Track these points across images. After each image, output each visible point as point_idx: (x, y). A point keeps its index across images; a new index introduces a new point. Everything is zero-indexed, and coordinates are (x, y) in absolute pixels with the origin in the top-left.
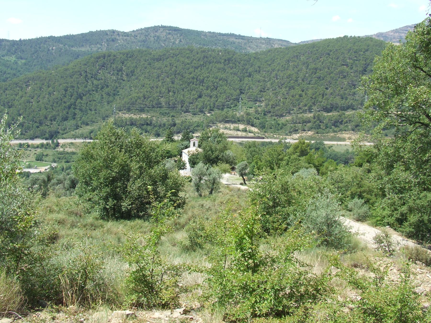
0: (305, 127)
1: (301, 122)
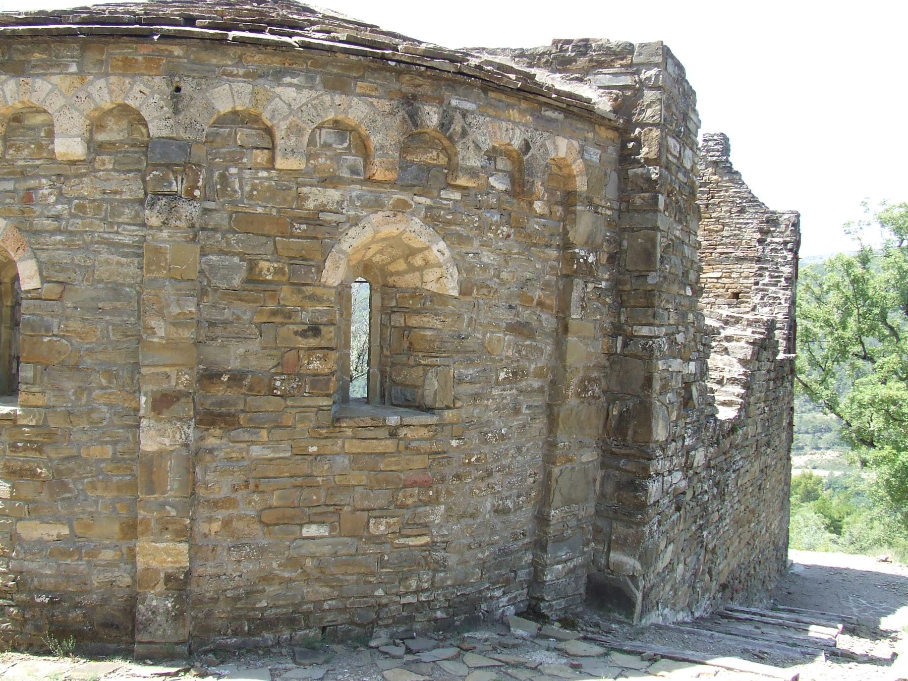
0: (819, 441)
1: (810, 431)
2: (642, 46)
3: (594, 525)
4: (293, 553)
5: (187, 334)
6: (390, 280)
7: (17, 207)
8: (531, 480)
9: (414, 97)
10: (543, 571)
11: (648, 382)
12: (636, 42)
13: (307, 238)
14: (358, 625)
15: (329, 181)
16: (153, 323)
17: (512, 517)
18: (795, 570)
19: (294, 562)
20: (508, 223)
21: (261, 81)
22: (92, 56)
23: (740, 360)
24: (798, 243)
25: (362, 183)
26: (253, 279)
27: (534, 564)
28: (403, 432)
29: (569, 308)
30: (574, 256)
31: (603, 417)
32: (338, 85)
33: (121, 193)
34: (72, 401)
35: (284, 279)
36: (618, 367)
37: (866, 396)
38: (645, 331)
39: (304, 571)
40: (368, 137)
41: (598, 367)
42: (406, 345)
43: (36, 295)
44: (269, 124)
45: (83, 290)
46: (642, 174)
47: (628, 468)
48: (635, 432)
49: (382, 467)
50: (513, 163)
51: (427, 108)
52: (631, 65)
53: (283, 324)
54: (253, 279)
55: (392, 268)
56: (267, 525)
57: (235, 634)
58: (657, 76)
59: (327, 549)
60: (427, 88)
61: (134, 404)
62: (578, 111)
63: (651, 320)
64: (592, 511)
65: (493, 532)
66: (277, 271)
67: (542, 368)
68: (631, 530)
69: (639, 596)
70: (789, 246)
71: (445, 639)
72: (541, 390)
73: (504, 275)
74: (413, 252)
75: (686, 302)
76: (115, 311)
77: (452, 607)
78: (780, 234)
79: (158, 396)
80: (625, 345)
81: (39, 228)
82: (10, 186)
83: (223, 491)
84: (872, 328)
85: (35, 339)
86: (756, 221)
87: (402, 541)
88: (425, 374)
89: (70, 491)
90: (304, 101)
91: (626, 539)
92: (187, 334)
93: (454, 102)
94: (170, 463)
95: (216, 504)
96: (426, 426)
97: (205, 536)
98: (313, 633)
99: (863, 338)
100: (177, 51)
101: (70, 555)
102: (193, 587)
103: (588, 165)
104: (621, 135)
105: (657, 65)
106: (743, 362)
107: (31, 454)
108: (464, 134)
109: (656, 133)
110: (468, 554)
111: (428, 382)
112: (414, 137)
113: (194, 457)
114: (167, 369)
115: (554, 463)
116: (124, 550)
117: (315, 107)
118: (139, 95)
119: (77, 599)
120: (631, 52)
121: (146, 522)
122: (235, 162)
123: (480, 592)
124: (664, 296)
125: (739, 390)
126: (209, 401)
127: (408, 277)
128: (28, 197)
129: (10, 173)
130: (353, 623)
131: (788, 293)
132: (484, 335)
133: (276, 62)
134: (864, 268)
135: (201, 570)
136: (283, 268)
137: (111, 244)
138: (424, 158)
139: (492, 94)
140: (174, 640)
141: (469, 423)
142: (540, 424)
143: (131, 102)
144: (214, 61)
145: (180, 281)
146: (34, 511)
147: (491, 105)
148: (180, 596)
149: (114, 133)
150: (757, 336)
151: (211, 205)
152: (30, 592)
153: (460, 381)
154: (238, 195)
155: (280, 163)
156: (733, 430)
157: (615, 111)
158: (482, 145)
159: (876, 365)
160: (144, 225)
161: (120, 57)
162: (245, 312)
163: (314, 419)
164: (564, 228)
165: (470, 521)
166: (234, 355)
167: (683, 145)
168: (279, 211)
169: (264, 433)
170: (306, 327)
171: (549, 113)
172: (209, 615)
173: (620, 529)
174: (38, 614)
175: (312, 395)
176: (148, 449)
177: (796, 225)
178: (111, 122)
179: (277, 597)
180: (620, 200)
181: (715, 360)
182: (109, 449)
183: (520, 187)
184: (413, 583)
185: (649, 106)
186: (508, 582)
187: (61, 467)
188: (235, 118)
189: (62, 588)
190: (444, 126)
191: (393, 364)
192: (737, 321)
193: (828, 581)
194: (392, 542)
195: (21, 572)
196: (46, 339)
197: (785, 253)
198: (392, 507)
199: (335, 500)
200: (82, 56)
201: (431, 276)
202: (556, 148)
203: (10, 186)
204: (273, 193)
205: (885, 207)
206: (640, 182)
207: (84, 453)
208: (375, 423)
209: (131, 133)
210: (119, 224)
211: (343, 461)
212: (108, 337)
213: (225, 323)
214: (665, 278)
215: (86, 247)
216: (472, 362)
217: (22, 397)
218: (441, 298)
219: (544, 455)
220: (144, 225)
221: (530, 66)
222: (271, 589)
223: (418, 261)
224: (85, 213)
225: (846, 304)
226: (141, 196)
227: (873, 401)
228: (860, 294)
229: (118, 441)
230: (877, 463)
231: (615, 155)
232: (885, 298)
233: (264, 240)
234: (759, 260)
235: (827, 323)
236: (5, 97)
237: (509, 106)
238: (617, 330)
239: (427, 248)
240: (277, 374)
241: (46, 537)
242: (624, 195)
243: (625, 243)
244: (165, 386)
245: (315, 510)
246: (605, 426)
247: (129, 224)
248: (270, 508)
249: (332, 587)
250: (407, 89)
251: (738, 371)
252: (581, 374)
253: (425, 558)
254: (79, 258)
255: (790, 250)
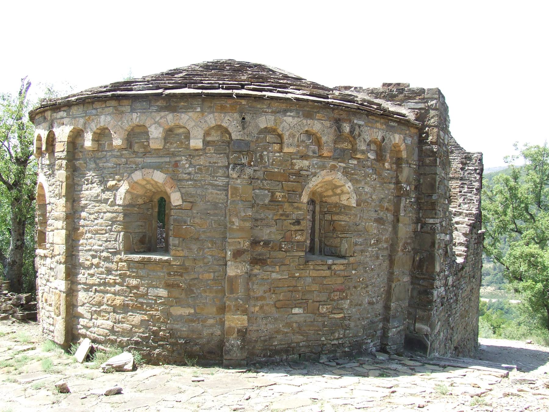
2: (429, 90)
3: (408, 311)
4: (288, 321)
5: (248, 224)
6: (324, 199)
7: (171, 169)
8: (383, 289)
9: (339, 120)
10: (388, 332)
11: (433, 244)
12: (426, 87)
13: (295, 182)
14: (314, 353)
15: (304, 157)
16: (234, 220)
17: (375, 306)
18: (482, 348)
19: (289, 325)
20: (375, 173)
21: (278, 115)
22: (207, 104)
23: (463, 234)
24: (482, 170)
25: (317, 157)
26: (273, 200)
27: (383, 328)
28: (333, 267)
29: (399, 211)
30: (401, 188)
31: (412, 261)
32: (309, 116)
33: (218, 163)
34: (195, 254)
35: (286, 200)
36: (418, 238)
37: (517, 252)
38: (431, 221)
39: (293, 329)
40: (321, 138)
41: (411, 238)
42: (332, 228)
43: (179, 208)
44: (280, 133)
45: (201, 205)
46: (429, 149)
47: (424, 284)
48: (427, 268)
49: (325, 283)
50: (377, 146)
51: (345, 125)
52: (424, 99)
53: (285, 220)
54: (273, 200)
55: (325, 194)
56: (278, 308)
57: (264, 356)
58: (436, 104)
59: (302, 319)
60: (344, 116)
61: (223, 255)
62: (403, 122)
63: (434, 216)
64: (407, 304)
65: (368, 313)
66: (284, 197)
67: (387, 238)
68: (426, 313)
69: (429, 343)
70: (478, 171)
71: (351, 360)
72: (387, 248)
73: (374, 197)
74: (337, 187)
75: (445, 207)
76: (215, 215)
77: (351, 346)
78: (473, 162)
79: (235, 252)
80: (422, 227)
81: (181, 178)
82: (168, 160)
83: (260, 293)
84: (521, 215)
85: (179, 227)
86: (459, 158)
87: (332, 316)
88: (341, 242)
89: (194, 293)
90: (295, 123)
91: (423, 317)
92: (248, 224)
93: (355, 121)
94: (240, 281)
95: (257, 299)
96: (343, 264)
97: (253, 313)
98: (296, 356)
99: (516, 221)
100: (244, 102)
101: (194, 322)
102: (248, 336)
103: (407, 145)
104: (419, 130)
105: (436, 99)
106: (465, 235)
107: (177, 277)
108: (360, 135)
109: (436, 130)
110: (358, 322)
111: (342, 245)
112: (339, 136)
113: (250, 276)
114: (239, 240)
115: (393, 282)
116: (218, 319)
117: (300, 125)
118: (228, 121)
119: (197, 341)
120: (424, 92)
121: (229, 306)
122: (266, 149)
123: (363, 340)
124: (439, 205)
125: (463, 248)
126: (255, 254)
127: (333, 198)
128: (176, 165)
129: (167, 154)
130: (312, 352)
131: (478, 196)
132: (365, 224)
133: (284, 106)
134: (516, 182)
135: (250, 328)
136: (285, 196)
137: (213, 185)
138: (342, 146)
139: (370, 117)
140: (242, 358)
141: (359, 263)
142: (386, 264)
143: (224, 125)
144: (259, 106)
145: (245, 202)
146: (179, 302)
147: (369, 122)
148: (244, 339)
149: (214, 137)
150: (471, 222)
151: (256, 168)
152: (176, 338)
153: (356, 244)
154: (267, 164)
155: (286, 150)
156: (463, 268)
157: (416, 120)
158: (366, 140)
159: (522, 236)
160: (228, 177)
161: (219, 105)
162: (270, 214)
163: (297, 261)
164: (397, 174)
165: (360, 307)
166: (265, 234)
167: (445, 133)
168: (284, 171)
169: (277, 267)
170: (294, 221)
171: (392, 124)
172: (254, 347)
173: (420, 313)
174: (179, 348)
175: (297, 251)
176: (231, 275)
177: (481, 160)
178: (213, 132)
179: (281, 340)
180: (419, 160)
181: (455, 234)
182: (212, 275)
183: (380, 158)
184: (337, 335)
185: (432, 118)
186: (373, 336)
187: (191, 283)
188: (267, 131)
189: (190, 336)
190: (352, 132)
191: (326, 237)
192: (461, 214)
193: (500, 353)
194: (328, 317)
195: (172, 330)
196: (184, 227)
197: (476, 175)
198: (329, 301)
199: (306, 297)
200: (202, 104)
201: (344, 198)
202: (395, 138)
203: (168, 160)
204: (282, 162)
205: (526, 147)
206: (428, 153)
207: (201, 277)
208: (323, 263)
209: (222, 137)
210: (217, 177)
211: (309, 280)
212: (212, 226)
213: (262, 219)
214: (439, 196)
215: (202, 187)
216: (361, 236)
217: (172, 253)
218: (349, 207)
219: (388, 278)
220: (228, 177)
221: (376, 98)
222: (279, 337)
223: (338, 191)
224: (202, 172)
225: (506, 202)
226: (227, 164)
227: (522, 255)
228: (514, 196)
229: (216, 271)
230: (525, 289)
231: (417, 140)
232: (527, 198)
233: (278, 183)
234: (461, 179)
235: (496, 212)
236: (167, 121)
237: (377, 122)
238: (418, 220)
239: (344, 185)
240: (283, 242)
241: (184, 314)
242: (421, 159)
243: (422, 181)
244: (239, 247)
245: (298, 302)
246: (413, 265)
247: (221, 177)
248: (279, 301)
249: (304, 336)
250: (336, 116)
251: (463, 239)
252: (403, 241)
253: (341, 323)
254: (199, 191)
255: (478, 174)
